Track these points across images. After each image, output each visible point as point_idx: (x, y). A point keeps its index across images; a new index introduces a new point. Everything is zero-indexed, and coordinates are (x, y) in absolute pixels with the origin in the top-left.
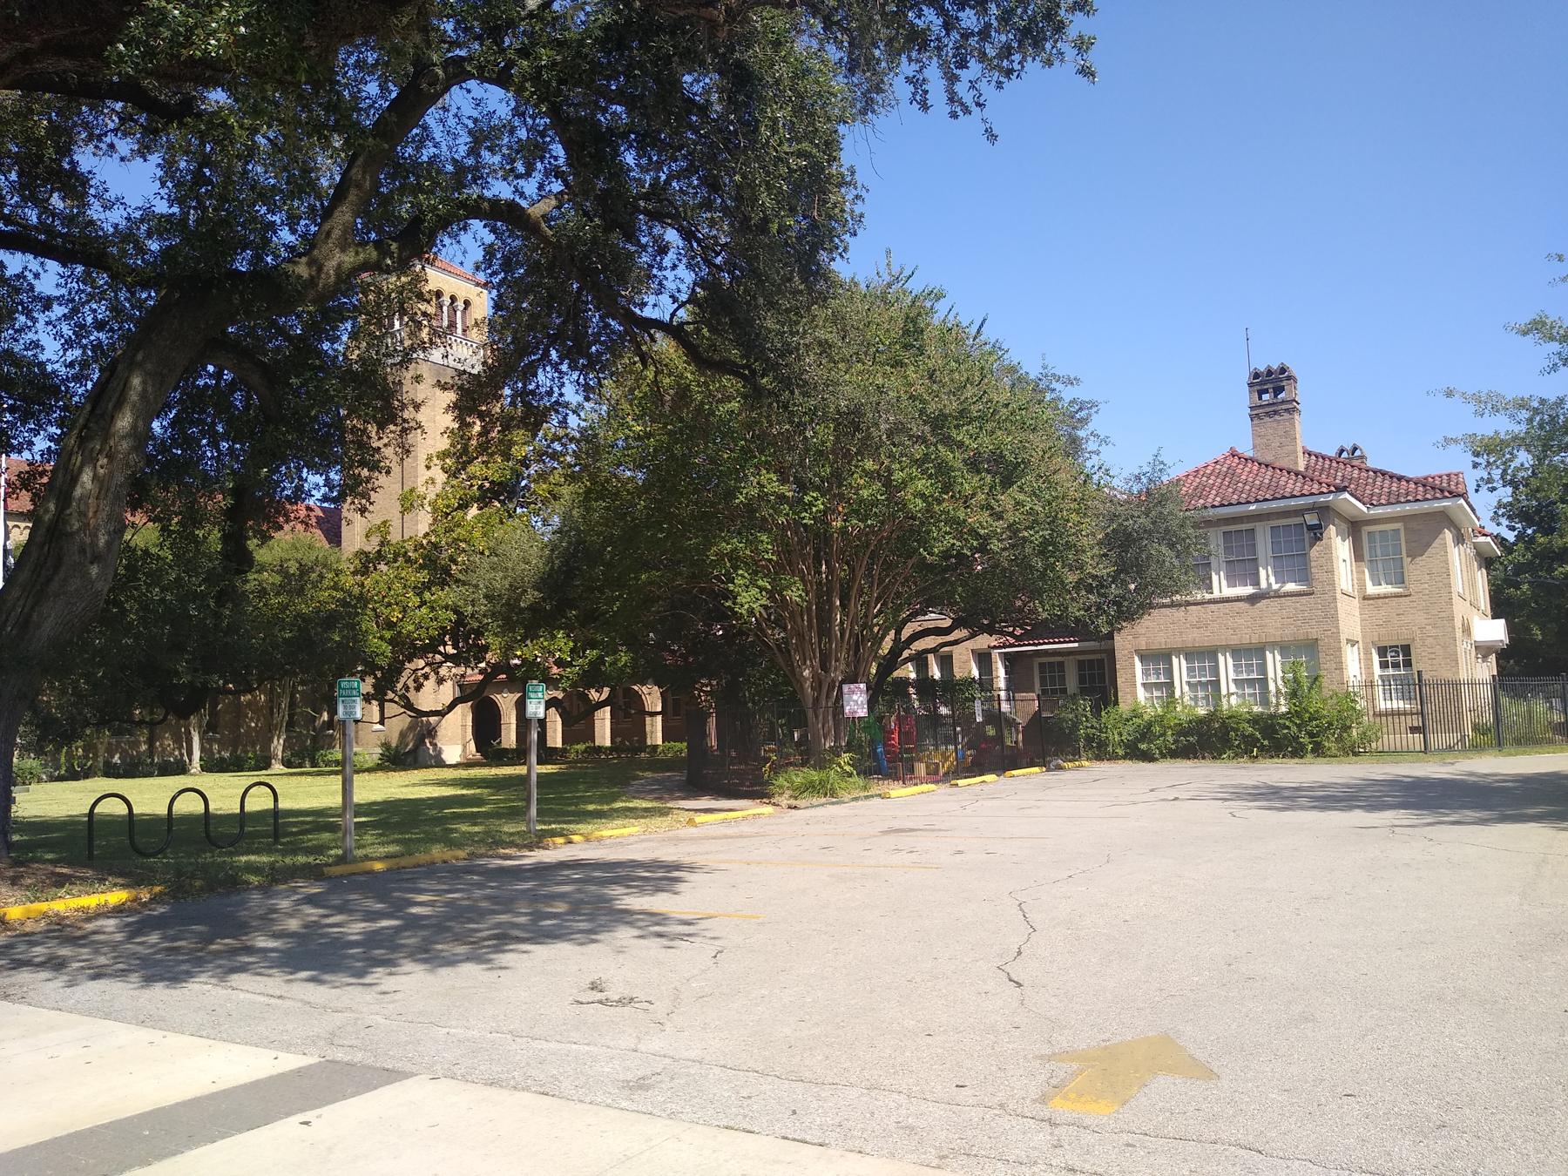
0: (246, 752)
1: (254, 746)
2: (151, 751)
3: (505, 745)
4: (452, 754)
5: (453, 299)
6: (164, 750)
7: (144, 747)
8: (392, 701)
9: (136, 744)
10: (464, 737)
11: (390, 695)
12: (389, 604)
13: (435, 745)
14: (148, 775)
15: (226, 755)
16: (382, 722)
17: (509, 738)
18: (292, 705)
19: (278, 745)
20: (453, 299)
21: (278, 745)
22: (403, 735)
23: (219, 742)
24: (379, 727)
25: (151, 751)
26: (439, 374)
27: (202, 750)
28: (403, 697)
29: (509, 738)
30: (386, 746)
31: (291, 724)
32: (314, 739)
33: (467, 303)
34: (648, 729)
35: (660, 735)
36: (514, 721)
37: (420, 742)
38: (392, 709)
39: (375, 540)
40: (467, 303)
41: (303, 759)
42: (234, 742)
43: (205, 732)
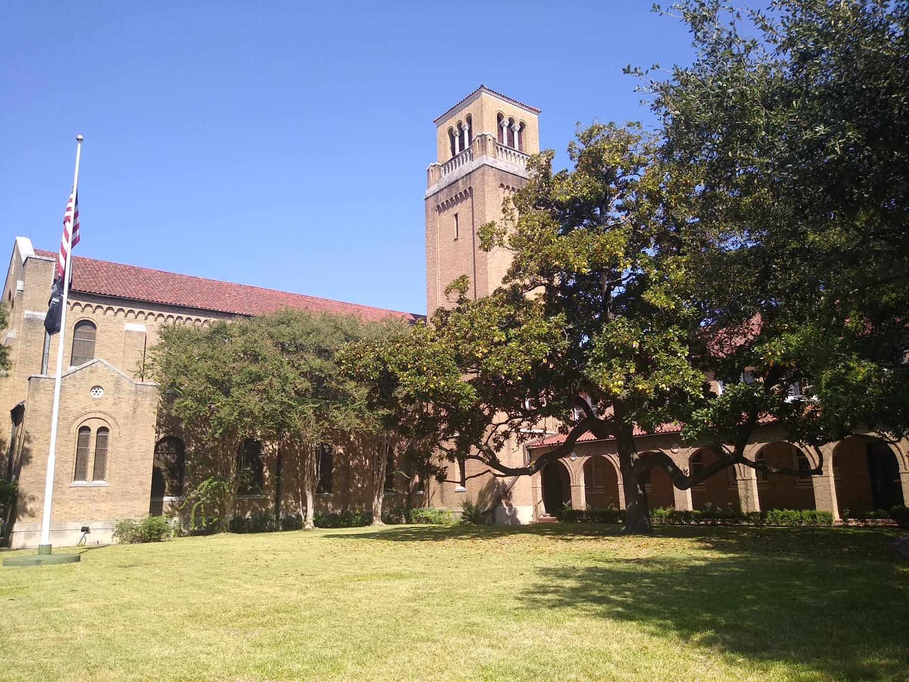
0: (354, 509)
1: (360, 504)
2: (277, 510)
3: (575, 507)
4: (526, 514)
5: (511, 121)
6: (287, 507)
7: (271, 505)
8: (477, 457)
9: (264, 502)
10: (535, 498)
11: (474, 450)
12: (473, 339)
13: (510, 506)
14: (271, 530)
15: (339, 512)
16: (463, 483)
17: (579, 500)
18: (390, 468)
19: (378, 504)
20: (511, 121)
21: (378, 504)
22: (482, 495)
23: (334, 501)
24: (459, 487)
25: (277, 510)
26: (502, 179)
27: (316, 508)
28: (489, 453)
29: (579, 500)
30: (467, 505)
31: (389, 485)
32: (409, 498)
33: (522, 125)
34: (741, 493)
35: (757, 500)
36: (582, 483)
37: (497, 502)
38: (474, 467)
39: (455, 296)
40: (522, 125)
41: (400, 515)
42: (344, 501)
43: (318, 491)
